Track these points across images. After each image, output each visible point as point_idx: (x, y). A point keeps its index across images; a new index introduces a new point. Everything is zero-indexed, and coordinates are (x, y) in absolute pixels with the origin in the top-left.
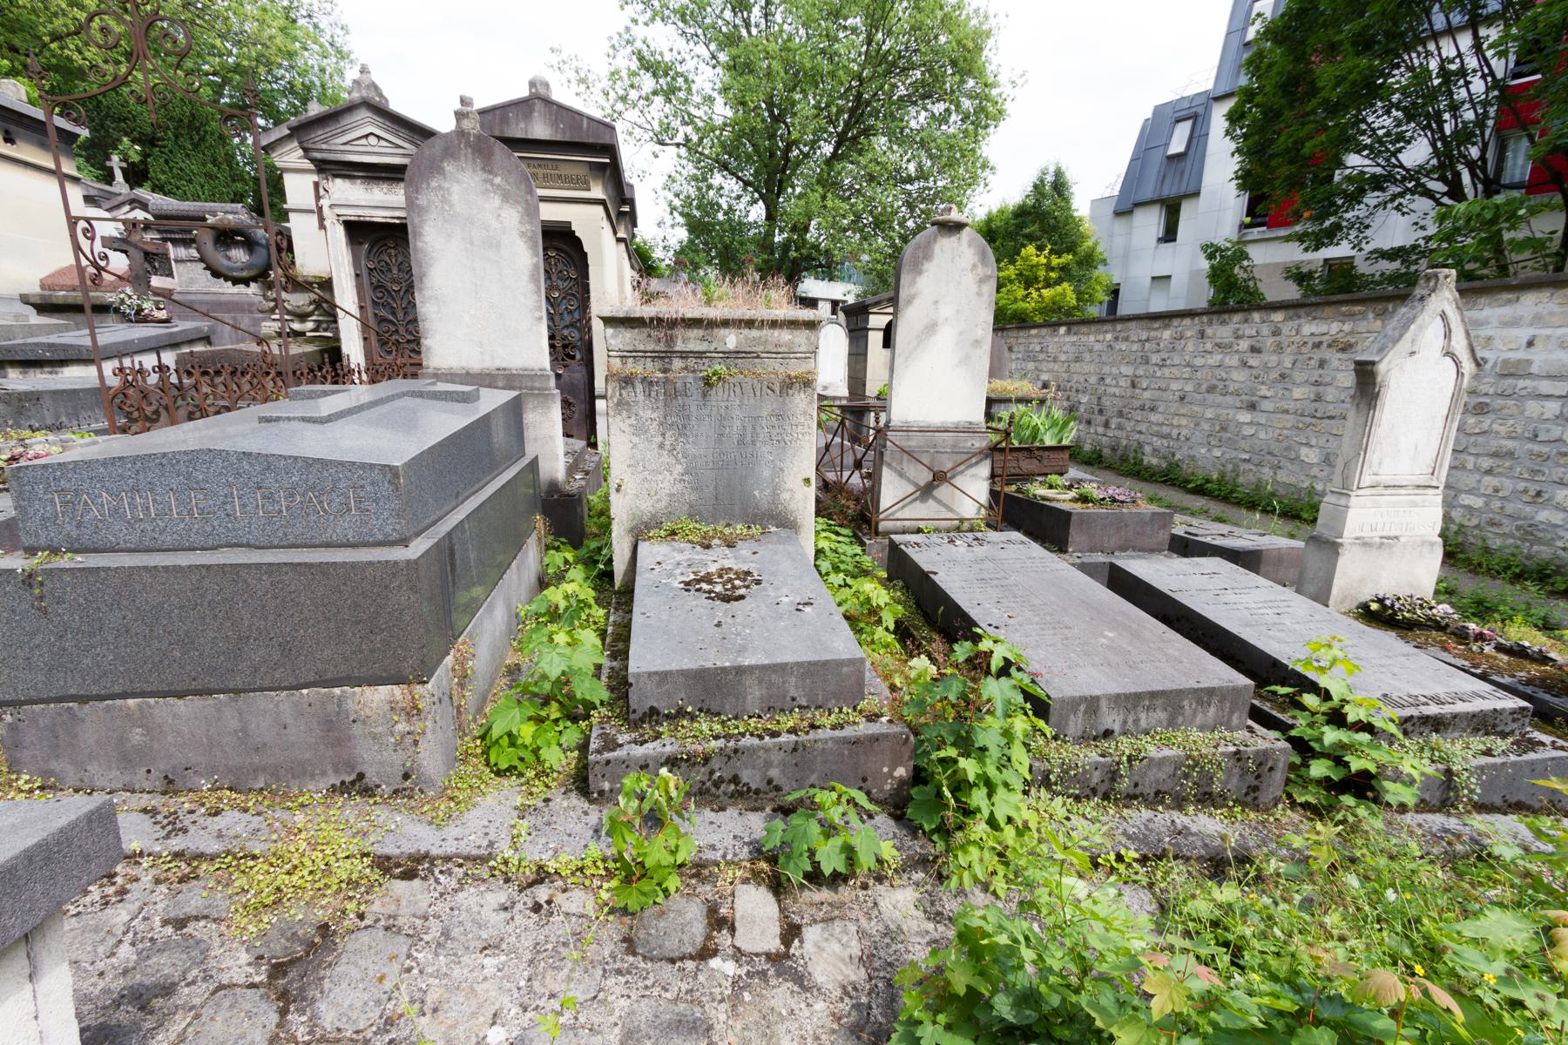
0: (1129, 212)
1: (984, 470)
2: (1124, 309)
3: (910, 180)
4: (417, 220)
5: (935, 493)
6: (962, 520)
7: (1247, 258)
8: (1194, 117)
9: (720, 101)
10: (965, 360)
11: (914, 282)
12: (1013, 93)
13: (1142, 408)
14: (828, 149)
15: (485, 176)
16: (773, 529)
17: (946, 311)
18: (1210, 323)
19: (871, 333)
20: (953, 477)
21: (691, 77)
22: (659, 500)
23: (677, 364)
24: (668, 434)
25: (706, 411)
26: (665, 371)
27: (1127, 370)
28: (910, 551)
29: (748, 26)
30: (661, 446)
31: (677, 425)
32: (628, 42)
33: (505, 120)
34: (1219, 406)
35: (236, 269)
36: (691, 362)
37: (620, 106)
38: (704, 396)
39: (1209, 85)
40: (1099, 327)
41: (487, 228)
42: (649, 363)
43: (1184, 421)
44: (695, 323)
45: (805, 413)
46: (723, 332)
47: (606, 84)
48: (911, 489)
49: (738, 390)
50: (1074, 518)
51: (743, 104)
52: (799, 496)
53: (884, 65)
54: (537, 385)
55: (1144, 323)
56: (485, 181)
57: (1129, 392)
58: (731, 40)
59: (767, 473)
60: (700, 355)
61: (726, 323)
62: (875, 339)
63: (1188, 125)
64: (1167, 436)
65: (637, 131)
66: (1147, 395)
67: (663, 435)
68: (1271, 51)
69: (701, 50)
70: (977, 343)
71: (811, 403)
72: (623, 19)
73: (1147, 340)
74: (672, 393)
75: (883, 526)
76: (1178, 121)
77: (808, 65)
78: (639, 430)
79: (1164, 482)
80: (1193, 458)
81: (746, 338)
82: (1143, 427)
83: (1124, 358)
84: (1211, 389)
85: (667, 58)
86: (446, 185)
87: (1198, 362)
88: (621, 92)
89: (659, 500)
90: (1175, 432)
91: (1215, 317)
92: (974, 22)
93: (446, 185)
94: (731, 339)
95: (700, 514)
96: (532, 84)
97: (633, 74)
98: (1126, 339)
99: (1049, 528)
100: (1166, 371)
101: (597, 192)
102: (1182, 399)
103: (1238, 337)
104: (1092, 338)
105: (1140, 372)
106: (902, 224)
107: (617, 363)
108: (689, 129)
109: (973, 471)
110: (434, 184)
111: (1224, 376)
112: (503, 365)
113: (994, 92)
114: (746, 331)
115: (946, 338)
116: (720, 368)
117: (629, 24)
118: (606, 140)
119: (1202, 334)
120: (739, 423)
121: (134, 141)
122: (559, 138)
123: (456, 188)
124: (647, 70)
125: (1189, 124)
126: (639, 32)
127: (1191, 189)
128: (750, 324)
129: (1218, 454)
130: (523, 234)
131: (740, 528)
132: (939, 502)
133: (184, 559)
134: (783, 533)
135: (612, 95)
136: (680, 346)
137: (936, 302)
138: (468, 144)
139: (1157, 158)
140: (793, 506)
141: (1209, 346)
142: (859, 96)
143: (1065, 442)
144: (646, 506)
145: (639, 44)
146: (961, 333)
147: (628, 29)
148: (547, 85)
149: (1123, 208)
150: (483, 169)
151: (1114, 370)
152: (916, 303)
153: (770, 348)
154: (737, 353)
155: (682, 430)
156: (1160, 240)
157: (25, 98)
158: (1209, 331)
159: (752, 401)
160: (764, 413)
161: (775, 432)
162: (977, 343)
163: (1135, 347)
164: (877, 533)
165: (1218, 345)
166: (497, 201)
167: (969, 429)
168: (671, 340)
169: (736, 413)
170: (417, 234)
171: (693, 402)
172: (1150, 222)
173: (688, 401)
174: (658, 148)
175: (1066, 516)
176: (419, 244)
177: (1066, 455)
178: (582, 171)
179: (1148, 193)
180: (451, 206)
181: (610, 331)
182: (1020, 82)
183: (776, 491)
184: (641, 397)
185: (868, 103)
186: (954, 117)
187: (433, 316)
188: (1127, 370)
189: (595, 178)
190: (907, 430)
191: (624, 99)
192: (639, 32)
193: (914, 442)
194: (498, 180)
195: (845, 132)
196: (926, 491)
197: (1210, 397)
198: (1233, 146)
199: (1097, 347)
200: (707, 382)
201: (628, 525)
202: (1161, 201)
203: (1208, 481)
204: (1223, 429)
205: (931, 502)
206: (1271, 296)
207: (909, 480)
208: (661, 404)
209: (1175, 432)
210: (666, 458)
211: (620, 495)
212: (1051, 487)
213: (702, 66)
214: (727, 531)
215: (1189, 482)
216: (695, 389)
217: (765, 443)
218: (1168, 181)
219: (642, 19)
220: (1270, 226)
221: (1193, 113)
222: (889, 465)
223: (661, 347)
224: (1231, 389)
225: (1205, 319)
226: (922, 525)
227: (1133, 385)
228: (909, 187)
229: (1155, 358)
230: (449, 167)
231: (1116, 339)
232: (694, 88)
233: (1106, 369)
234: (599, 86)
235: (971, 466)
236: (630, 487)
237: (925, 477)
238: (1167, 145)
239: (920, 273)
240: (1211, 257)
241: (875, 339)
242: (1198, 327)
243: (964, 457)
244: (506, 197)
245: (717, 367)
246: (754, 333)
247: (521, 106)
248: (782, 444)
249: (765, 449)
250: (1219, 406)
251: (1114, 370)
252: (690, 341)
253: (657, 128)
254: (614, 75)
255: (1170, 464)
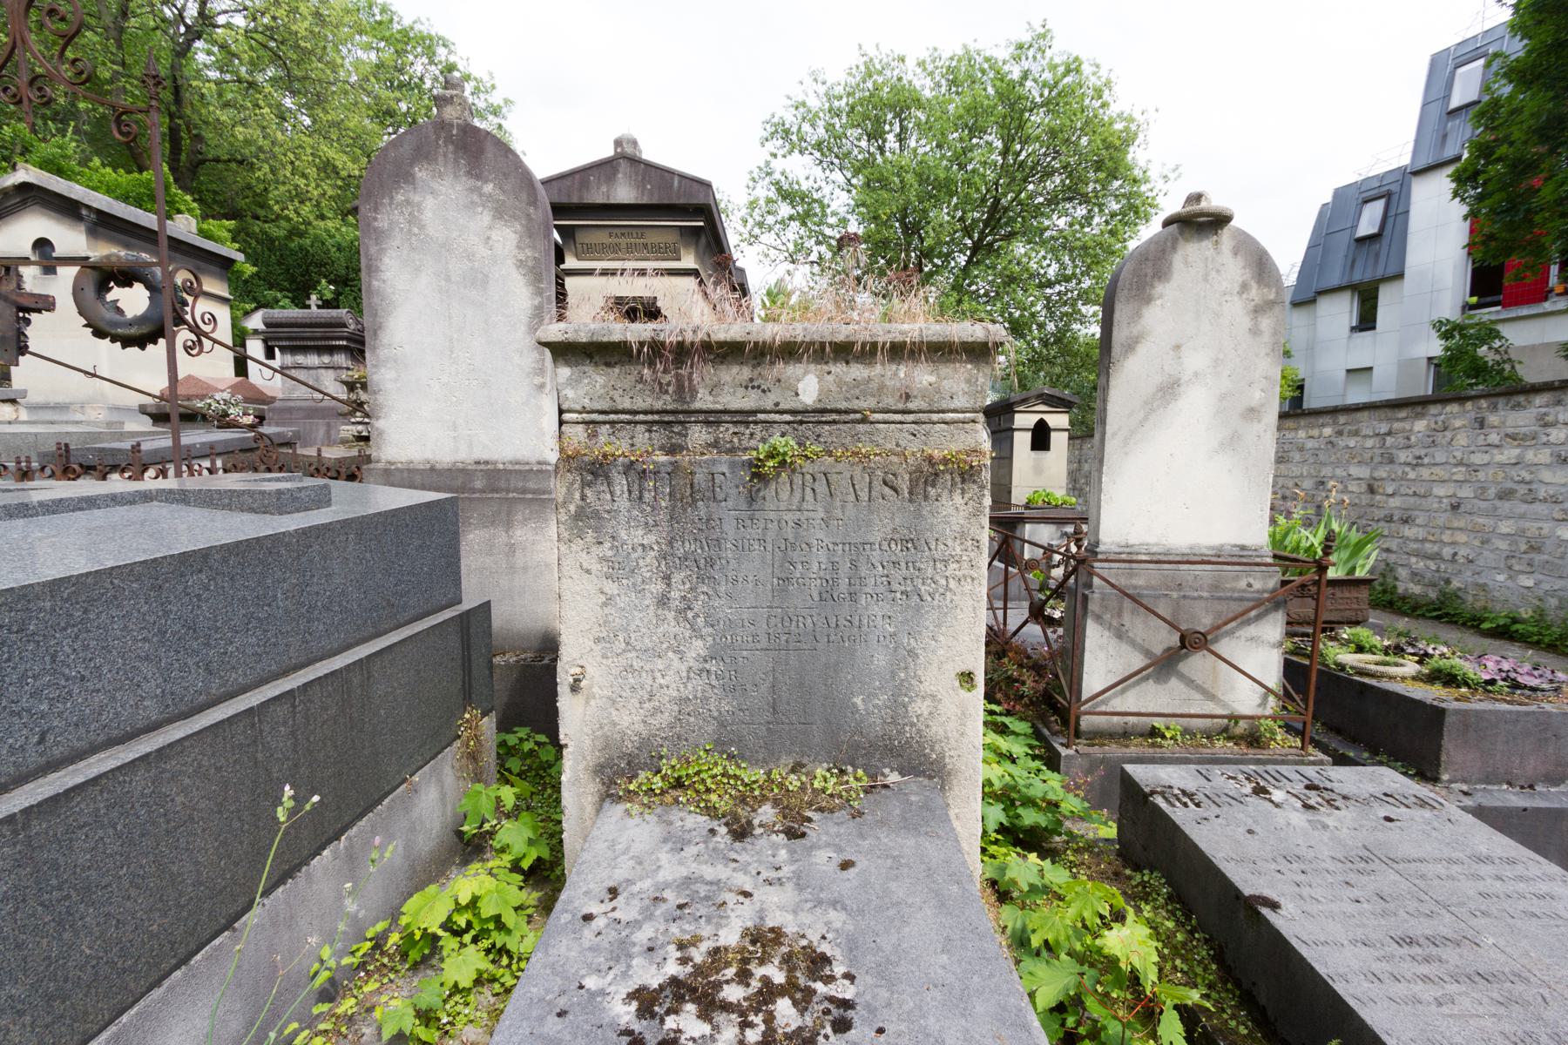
0: (1312, 301)
1: (1272, 629)
2: (1310, 402)
3: (1050, 284)
4: (373, 250)
5: (1183, 667)
6: (1235, 718)
7: (1498, 336)
8: (1388, 196)
9: (853, 219)
10: (1232, 442)
11: (1138, 315)
12: (1165, 188)
13: (1389, 519)
14: (962, 260)
15: (472, 182)
16: (893, 777)
17: (1195, 361)
18: (1494, 408)
19: (1016, 434)
20: (1216, 640)
21: (826, 201)
22: (657, 711)
23: (698, 435)
24: (677, 578)
25: (754, 532)
26: (672, 450)
27: (1364, 472)
28: (1181, 816)
29: (881, 149)
30: (663, 601)
31: (693, 555)
32: (768, 174)
33: (585, 184)
34: (1522, 516)
35: (131, 324)
36: (726, 432)
37: (757, 231)
38: (752, 499)
39: (1406, 160)
40: (1312, 420)
41: (470, 257)
42: (641, 436)
43: (1461, 537)
44: (729, 352)
45: (962, 536)
46: (791, 370)
47: (744, 211)
48: (1138, 661)
49: (821, 487)
50: (1449, 720)
51: (876, 218)
52: (949, 708)
53: (1018, 173)
54: (531, 485)
55: (1381, 413)
56: (472, 190)
57: (1365, 499)
58: (868, 163)
59: (881, 660)
60: (744, 417)
61: (790, 351)
62: (1022, 441)
63: (1379, 205)
64: (1436, 557)
65: (772, 252)
66: (1395, 502)
67: (667, 578)
68: (1511, 97)
69: (838, 176)
70: (1252, 413)
71: (976, 514)
72: (762, 156)
73: (1389, 433)
74: (685, 494)
75: (1086, 722)
76: (1366, 201)
77: (942, 176)
78: (617, 568)
79: (1438, 618)
80: (1483, 587)
81: (840, 383)
82: (1393, 544)
83: (1353, 456)
84: (1505, 495)
85: (804, 188)
86: (417, 198)
87: (1478, 459)
88: (758, 218)
89: (657, 711)
90: (1447, 552)
91: (1501, 401)
92: (1118, 126)
93: (417, 198)
94: (809, 385)
95: (739, 741)
96: (618, 143)
97: (769, 201)
98: (1356, 433)
99: (1400, 735)
100: (1425, 473)
101: (688, 261)
102: (1455, 507)
103: (1546, 425)
104: (1302, 434)
105: (1382, 473)
106: (1041, 326)
107: (577, 434)
108: (823, 248)
109: (1252, 630)
110: (400, 198)
111: (1528, 477)
112: (485, 456)
113: (1143, 188)
114: (838, 369)
115: (1195, 408)
116: (783, 442)
117: (769, 158)
118: (700, 199)
119: (1481, 423)
120: (822, 556)
121: (330, 282)
122: (645, 201)
123: (429, 203)
124: (784, 198)
125: (1380, 204)
126: (778, 165)
127: (1391, 271)
128: (843, 351)
129: (1530, 583)
130: (521, 264)
131: (822, 776)
132: (1190, 682)
133: (338, 662)
134: (916, 791)
135: (751, 221)
136: (704, 400)
137: (1178, 347)
138: (449, 139)
139: (1343, 242)
140: (936, 730)
141: (1494, 438)
142: (997, 201)
143: (1360, 573)
144: (630, 721)
145: (777, 176)
146: (1223, 397)
147: (768, 163)
148: (634, 143)
149: (1300, 298)
150: (469, 173)
151: (1339, 472)
152: (1142, 350)
153: (890, 401)
154: (820, 414)
155: (705, 570)
156: (1353, 329)
157: (194, 230)
158: (1493, 419)
159: (851, 510)
160: (876, 537)
161: (897, 575)
162: (1252, 413)
163: (1369, 443)
164: (1078, 734)
165: (1513, 437)
166: (486, 218)
167: (1241, 558)
168: (684, 390)
169: (818, 534)
170: (373, 270)
171: (729, 513)
172: (1339, 311)
173: (718, 511)
174: (791, 267)
175: (1436, 715)
176: (375, 283)
177: (1364, 594)
178: (670, 238)
179: (1335, 279)
180: (422, 227)
181: (565, 372)
182: (1172, 176)
183: (898, 707)
184: (623, 503)
185: (1006, 210)
186: (1096, 220)
187: (389, 385)
188: (1364, 472)
189: (686, 246)
190: (1128, 559)
191: (760, 225)
192: (778, 165)
193: (1141, 580)
194: (489, 188)
195: (981, 239)
196: (1164, 665)
197: (1505, 506)
198: (1465, 209)
199: (1310, 444)
200: (757, 474)
201: (592, 759)
202: (1352, 287)
203: (1515, 621)
204: (1532, 548)
205: (1174, 682)
206: (1530, 376)
207: (1133, 643)
208: (663, 516)
209: (1447, 552)
210: (671, 626)
211: (579, 699)
212: (1360, 649)
213: (837, 191)
214: (793, 782)
215: (1482, 620)
216: (732, 485)
217: (877, 597)
218: (1359, 264)
219: (781, 152)
220: (1505, 305)
221: (1391, 193)
222: (1098, 618)
223: (666, 402)
224: (1542, 494)
225: (1484, 403)
226: (1159, 723)
227: (1371, 490)
228: (1048, 291)
229: (1403, 456)
230: (421, 173)
231: (1340, 433)
232: (828, 211)
233: (1327, 471)
234: (739, 215)
235: (1249, 622)
236: (598, 677)
237: (1163, 639)
238: (1355, 227)
239: (1148, 300)
240: (1446, 336)
241: (1022, 441)
242: (1473, 415)
243: (1237, 607)
244: (500, 213)
245: (776, 440)
246: (857, 371)
247: (605, 169)
248: (913, 600)
249: (877, 610)
250: (1522, 516)
251: (1339, 472)
252: (724, 389)
253: (791, 247)
254: (752, 205)
255: (1444, 594)
